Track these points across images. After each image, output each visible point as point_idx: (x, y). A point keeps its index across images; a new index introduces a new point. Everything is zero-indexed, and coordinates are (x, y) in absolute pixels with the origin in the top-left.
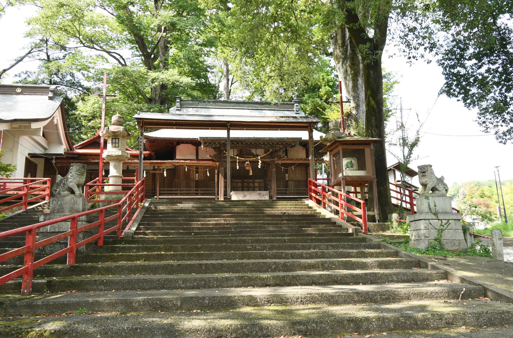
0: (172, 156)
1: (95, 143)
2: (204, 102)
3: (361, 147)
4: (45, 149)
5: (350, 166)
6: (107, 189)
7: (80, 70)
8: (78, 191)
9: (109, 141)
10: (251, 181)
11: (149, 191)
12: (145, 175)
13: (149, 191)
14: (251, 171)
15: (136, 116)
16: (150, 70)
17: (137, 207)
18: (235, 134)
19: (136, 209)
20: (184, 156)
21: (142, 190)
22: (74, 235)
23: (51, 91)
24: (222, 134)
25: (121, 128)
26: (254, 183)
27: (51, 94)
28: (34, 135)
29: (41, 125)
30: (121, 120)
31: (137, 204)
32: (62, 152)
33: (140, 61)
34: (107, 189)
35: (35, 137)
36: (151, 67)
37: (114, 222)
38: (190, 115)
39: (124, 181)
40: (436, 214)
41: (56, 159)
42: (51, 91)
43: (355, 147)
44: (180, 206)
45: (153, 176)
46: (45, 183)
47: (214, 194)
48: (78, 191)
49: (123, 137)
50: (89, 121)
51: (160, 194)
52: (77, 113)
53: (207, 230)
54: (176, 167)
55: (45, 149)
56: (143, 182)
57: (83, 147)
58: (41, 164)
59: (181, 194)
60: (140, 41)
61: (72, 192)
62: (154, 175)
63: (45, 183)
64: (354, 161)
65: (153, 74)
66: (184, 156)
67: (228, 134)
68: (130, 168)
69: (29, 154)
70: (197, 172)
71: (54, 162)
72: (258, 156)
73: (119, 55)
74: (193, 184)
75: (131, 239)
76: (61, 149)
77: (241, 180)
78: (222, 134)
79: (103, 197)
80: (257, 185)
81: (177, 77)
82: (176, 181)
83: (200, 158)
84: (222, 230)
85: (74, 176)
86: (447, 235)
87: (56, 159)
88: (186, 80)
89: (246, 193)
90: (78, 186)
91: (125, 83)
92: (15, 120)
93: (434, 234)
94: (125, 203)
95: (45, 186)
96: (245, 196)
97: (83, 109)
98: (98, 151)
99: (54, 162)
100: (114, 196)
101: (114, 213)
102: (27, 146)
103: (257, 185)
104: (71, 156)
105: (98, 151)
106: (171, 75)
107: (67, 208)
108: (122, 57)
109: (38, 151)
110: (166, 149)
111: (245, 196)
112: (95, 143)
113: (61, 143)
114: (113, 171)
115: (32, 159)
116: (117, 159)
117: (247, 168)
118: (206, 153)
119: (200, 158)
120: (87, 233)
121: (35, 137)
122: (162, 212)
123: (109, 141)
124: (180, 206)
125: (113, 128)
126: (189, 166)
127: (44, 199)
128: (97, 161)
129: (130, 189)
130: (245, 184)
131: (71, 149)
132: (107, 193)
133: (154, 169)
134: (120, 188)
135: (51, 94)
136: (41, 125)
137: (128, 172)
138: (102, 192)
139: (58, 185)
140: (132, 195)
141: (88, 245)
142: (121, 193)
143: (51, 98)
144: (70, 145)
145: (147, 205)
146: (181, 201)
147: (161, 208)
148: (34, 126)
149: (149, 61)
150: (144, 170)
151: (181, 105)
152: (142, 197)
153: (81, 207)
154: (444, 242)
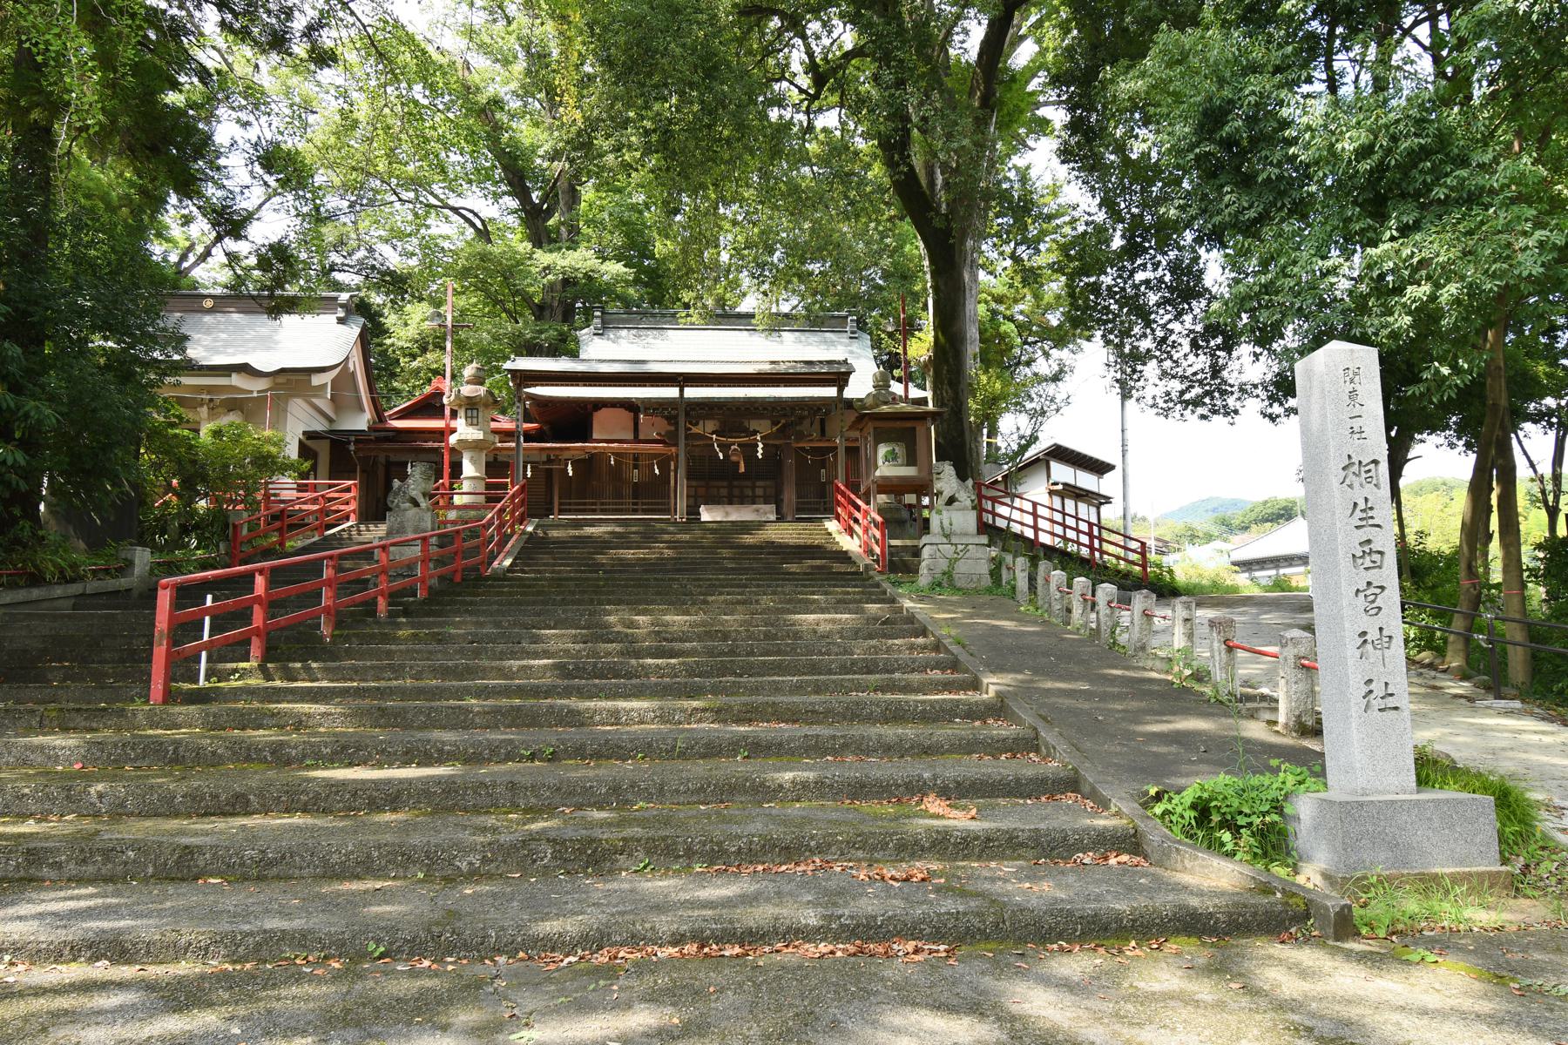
0: (585, 435)
1: (430, 406)
2: (653, 315)
3: (909, 424)
4: (331, 421)
5: (891, 457)
6: (457, 500)
7: (499, 517)
8: (424, 504)
9: (461, 413)
10: (748, 483)
11: (537, 502)
12: (529, 474)
13: (537, 502)
14: (742, 465)
15: (508, 365)
16: (540, 247)
17: (513, 532)
18: (692, 393)
19: (511, 536)
20: (608, 436)
21: (522, 502)
22: (425, 560)
23: (342, 306)
24: (671, 392)
25: (481, 390)
26: (753, 488)
27: (341, 314)
28: (315, 396)
30: (481, 374)
31: (512, 526)
33: (518, 222)
34: (457, 500)
35: (316, 401)
36: (540, 237)
37: (476, 550)
39: (489, 486)
40: (947, 536)
41: (357, 442)
42: (342, 306)
43: (898, 424)
44: (589, 530)
45: (547, 473)
46: (348, 490)
47: (667, 511)
48: (424, 504)
49: (486, 406)
50: (414, 357)
51: (561, 512)
52: (388, 342)
53: (624, 564)
54: (593, 455)
55: (331, 421)
56: (523, 487)
58: (323, 449)
59: (604, 511)
60: (515, 172)
61: (416, 504)
62: (549, 472)
63: (348, 490)
64: (900, 449)
65: (544, 258)
66: (608, 436)
67: (682, 392)
68: (500, 459)
69: (304, 433)
70: (636, 467)
71: (352, 447)
72: (755, 432)
73: (476, 215)
74: (627, 491)
75: (503, 576)
77: (715, 481)
78: (671, 392)
79: (452, 515)
80: (759, 492)
81: (593, 263)
82: (594, 484)
83: (641, 437)
84: (648, 566)
86: (962, 567)
87: (357, 442)
88: (614, 268)
89: (729, 508)
90: (424, 495)
91: (492, 278)
92: (283, 371)
93: (943, 565)
94: (490, 523)
95: (348, 495)
96: (727, 514)
97: (408, 324)
99: (352, 447)
100: (472, 513)
103: (759, 492)
104: (383, 434)
106: (579, 259)
107: (409, 527)
108: (476, 215)
109: (319, 426)
110: (571, 421)
111: (727, 514)
112: (430, 406)
113: (362, 410)
114: (469, 469)
115: (309, 443)
116: (475, 446)
117: (734, 458)
118: (652, 427)
119: (641, 437)
120: (440, 562)
121: (316, 401)
122: (560, 543)
123: (461, 413)
124: (589, 530)
125: (467, 390)
127: (347, 518)
128: (436, 445)
129: (499, 500)
130: (736, 492)
132: (459, 508)
133: (549, 461)
134: (482, 499)
135: (341, 314)
137: (496, 467)
138: (450, 505)
139: (397, 494)
140: (502, 510)
141: (441, 578)
142: (485, 508)
143: (341, 321)
145: (530, 529)
146: (592, 523)
147: (554, 533)
148: (316, 380)
149: (535, 222)
150: (525, 464)
151: (603, 322)
152: (522, 515)
153: (429, 526)
154: (956, 577)
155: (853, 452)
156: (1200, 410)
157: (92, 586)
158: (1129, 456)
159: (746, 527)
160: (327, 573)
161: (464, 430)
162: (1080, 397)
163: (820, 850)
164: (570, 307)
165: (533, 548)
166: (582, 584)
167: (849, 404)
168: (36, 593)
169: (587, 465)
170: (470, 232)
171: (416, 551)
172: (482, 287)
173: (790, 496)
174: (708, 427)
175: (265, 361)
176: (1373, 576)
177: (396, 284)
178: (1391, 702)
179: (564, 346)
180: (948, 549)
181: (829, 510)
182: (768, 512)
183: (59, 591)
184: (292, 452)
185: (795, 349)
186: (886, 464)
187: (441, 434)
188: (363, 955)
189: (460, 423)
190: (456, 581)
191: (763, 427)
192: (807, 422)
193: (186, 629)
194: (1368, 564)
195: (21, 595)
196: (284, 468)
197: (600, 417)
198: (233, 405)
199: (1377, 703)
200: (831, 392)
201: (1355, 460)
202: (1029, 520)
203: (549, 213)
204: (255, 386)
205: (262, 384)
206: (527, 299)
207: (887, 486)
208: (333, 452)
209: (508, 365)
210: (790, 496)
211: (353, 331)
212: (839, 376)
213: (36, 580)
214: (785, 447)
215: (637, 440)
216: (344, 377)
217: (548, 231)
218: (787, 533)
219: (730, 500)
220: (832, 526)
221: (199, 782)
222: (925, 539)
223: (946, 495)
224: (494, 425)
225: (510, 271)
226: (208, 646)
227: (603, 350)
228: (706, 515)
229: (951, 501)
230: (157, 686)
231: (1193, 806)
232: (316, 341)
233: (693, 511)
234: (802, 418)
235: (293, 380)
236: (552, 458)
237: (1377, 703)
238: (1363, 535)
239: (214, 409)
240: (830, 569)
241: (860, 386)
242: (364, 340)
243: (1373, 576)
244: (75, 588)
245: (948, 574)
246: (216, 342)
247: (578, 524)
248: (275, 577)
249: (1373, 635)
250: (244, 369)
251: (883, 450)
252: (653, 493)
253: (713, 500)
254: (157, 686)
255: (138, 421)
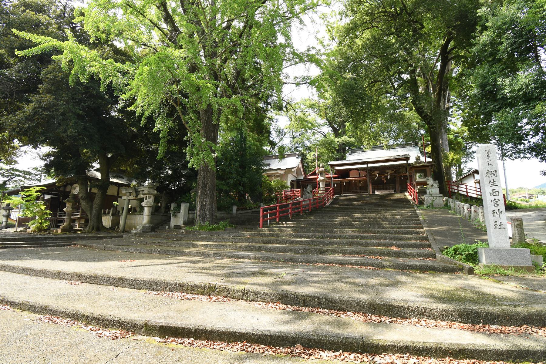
5: (420, 176)
15: (329, 163)
18: (369, 165)
20: (353, 177)
22: (310, 204)
24: (365, 166)
25: (323, 169)
29: (295, 169)
32: (303, 178)
37: (322, 202)
38: (171, 263)
57: (310, 175)
65: (337, 140)
75: (327, 207)
76: (302, 177)
77: (379, 184)
78: (365, 166)
79: (319, 195)
80: (391, 187)
82: (350, 187)
85: (309, 188)
88: (353, 139)
91: (327, 144)
93: (430, 202)
97: (310, 156)
98: (316, 177)
101: (322, 200)
102: (291, 178)
105: (316, 177)
106: (345, 138)
110: (345, 174)
112: (314, 174)
114: (321, 185)
116: (322, 181)
120: (314, 204)
125: (320, 169)
126: (355, 180)
131: (306, 177)
136: (295, 169)
137: (327, 185)
138: (318, 193)
144: (305, 174)
146: (349, 196)
148: (293, 170)
155: (411, 176)
156: (512, 158)
157: (254, 210)
158: (506, 171)
159: (387, 195)
160: (290, 206)
161: (320, 178)
162: (480, 157)
163: (364, 253)
164: (342, 151)
165: (336, 201)
166: (347, 208)
167: (409, 164)
168: (246, 211)
169: (349, 183)
170: (323, 136)
171: (308, 202)
172: (325, 147)
173: (398, 187)
174: (376, 172)
175: (283, 168)
176: (497, 197)
177: (309, 149)
178: (502, 227)
179: (343, 158)
180: (431, 198)
181: (406, 191)
182: (393, 192)
183: (249, 211)
184: (289, 184)
185: (400, 152)
186: (418, 178)
187: (316, 179)
188: (281, 261)
189: (319, 176)
190: (318, 208)
191: (390, 172)
192: (401, 170)
193: (265, 216)
194: (494, 194)
195: (243, 212)
196: (287, 187)
197: (351, 173)
198: (278, 176)
199: (498, 227)
200: (405, 162)
201: (490, 171)
202: (465, 190)
203: (339, 130)
204: (282, 172)
205: (283, 172)
206: (335, 148)
207: (419, 183)
208: (298, 184)
209: (329, 163)
210: (398, 187)
211: (299, 159)
212: (407, 159)
213: (246, 209)
214: (397, 176)
215: (360, 177)
216: (298, 169)
217: (339, 134)
218: (397, 196)
219: (384, 189)
220: (407, 194)
221: (265, 239)
222: (425, 196)
223: (430, 184)
224: (327, 176)
225: (331, 143)
226: (269, 219)
227: (351, 158)
228: (377, 193)
229: (432, 186)
230: (261, 225)
231: (453, 250)
232: (293, 162)
233: (373, 192)
234: (400, 169)
235: (288, 170)
236: (341, 182)
237: (498, 227)
238: (493, 188)
239: (275, 177)
240: (405, 203)
241: (412, 160)
242: (302, 161)
243: (497, 197)
244: (252, 210)
245: (432, 204)
246: (275, 164)
247: (347, 196)
248: (281, 207)
249: (496, 211)
250: (280, 169)
251: (418, 175)
252: (364, 189)
253: (378, 189)
254: (261, 225)
255: (260, 180)
